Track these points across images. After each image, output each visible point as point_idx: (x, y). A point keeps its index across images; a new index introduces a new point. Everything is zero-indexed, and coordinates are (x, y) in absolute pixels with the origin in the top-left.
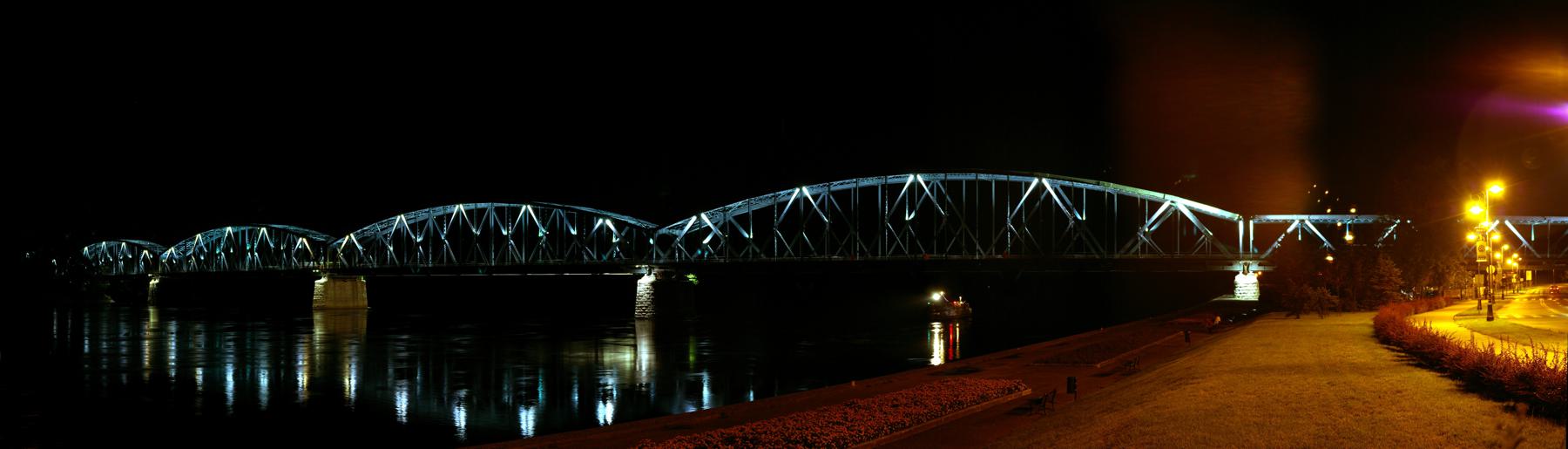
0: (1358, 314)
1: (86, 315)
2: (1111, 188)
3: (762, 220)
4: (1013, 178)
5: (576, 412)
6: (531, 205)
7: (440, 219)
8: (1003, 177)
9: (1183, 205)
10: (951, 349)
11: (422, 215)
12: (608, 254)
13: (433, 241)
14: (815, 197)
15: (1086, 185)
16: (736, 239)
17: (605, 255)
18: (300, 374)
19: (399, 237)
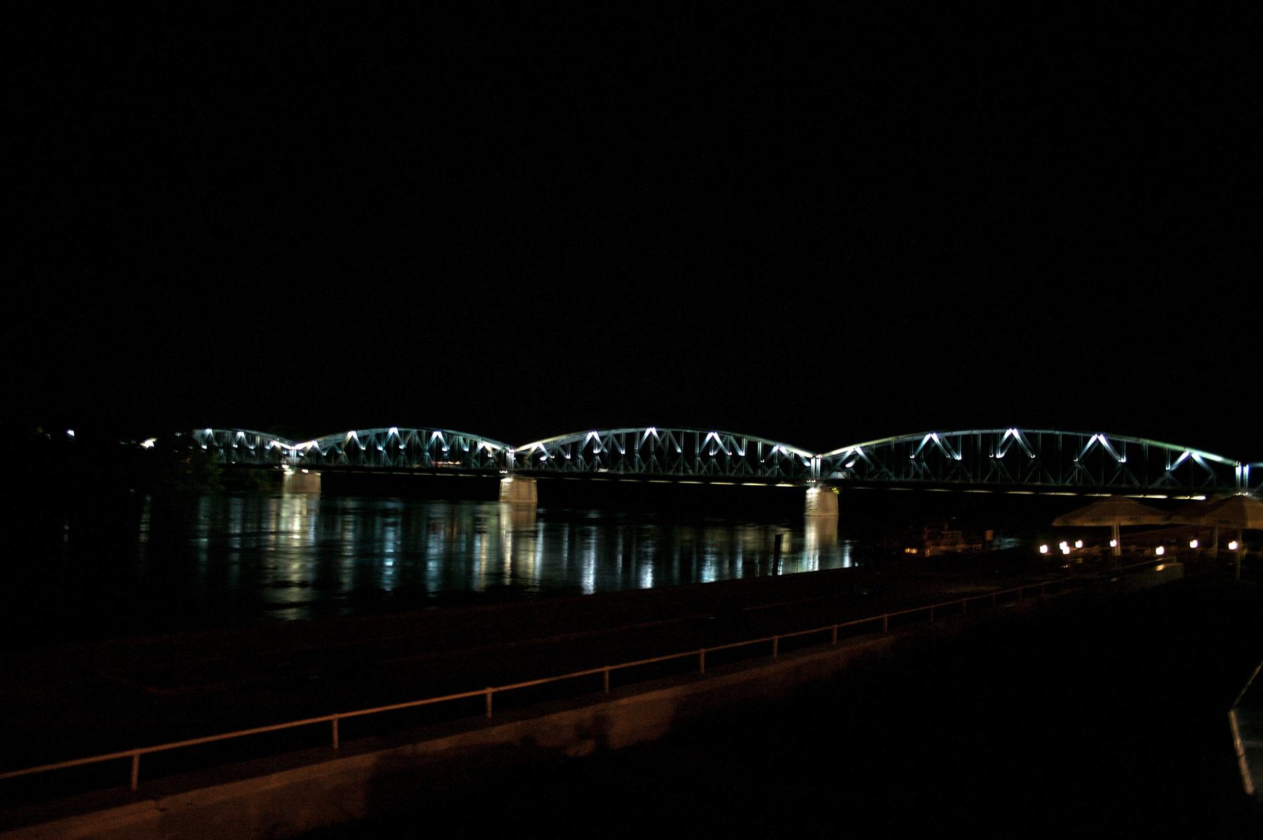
0: (837, 522)
1: (912, 489)
2: (1147, 442)
3: (574, 447)
4: (995, 431)
5: (295, 569)
6: (1018, 429)
7: (378, 436)
8: (988, 431)
9: (1197, 455)
10: (526, 534)
11: (366, 432)
12: (677, 463)
13: (372, 449)
14: (601, 438)
15: (1126, 440)
16: (560, 459)
17: (674, 464)
18: (773, 541)
19: (352, 446)
